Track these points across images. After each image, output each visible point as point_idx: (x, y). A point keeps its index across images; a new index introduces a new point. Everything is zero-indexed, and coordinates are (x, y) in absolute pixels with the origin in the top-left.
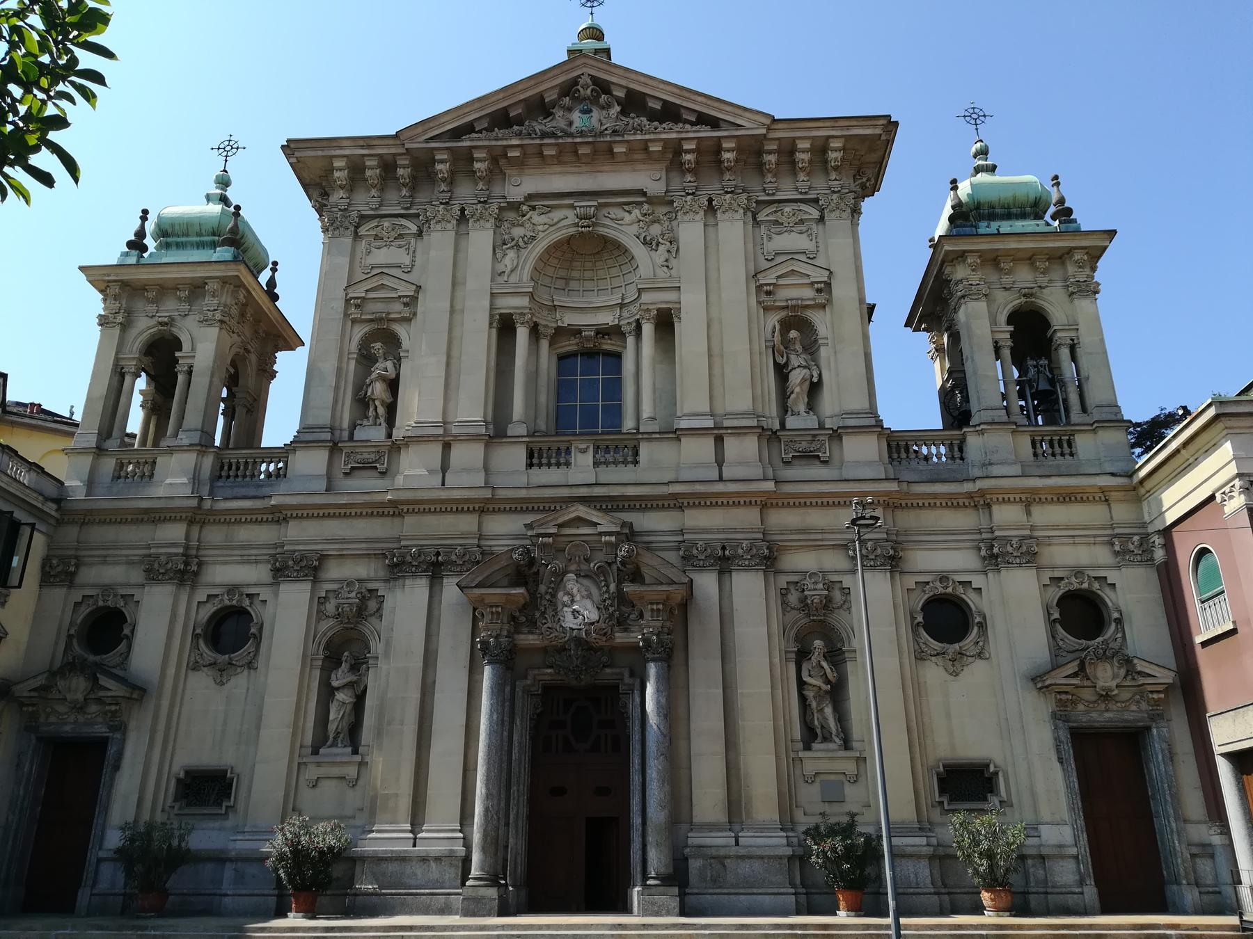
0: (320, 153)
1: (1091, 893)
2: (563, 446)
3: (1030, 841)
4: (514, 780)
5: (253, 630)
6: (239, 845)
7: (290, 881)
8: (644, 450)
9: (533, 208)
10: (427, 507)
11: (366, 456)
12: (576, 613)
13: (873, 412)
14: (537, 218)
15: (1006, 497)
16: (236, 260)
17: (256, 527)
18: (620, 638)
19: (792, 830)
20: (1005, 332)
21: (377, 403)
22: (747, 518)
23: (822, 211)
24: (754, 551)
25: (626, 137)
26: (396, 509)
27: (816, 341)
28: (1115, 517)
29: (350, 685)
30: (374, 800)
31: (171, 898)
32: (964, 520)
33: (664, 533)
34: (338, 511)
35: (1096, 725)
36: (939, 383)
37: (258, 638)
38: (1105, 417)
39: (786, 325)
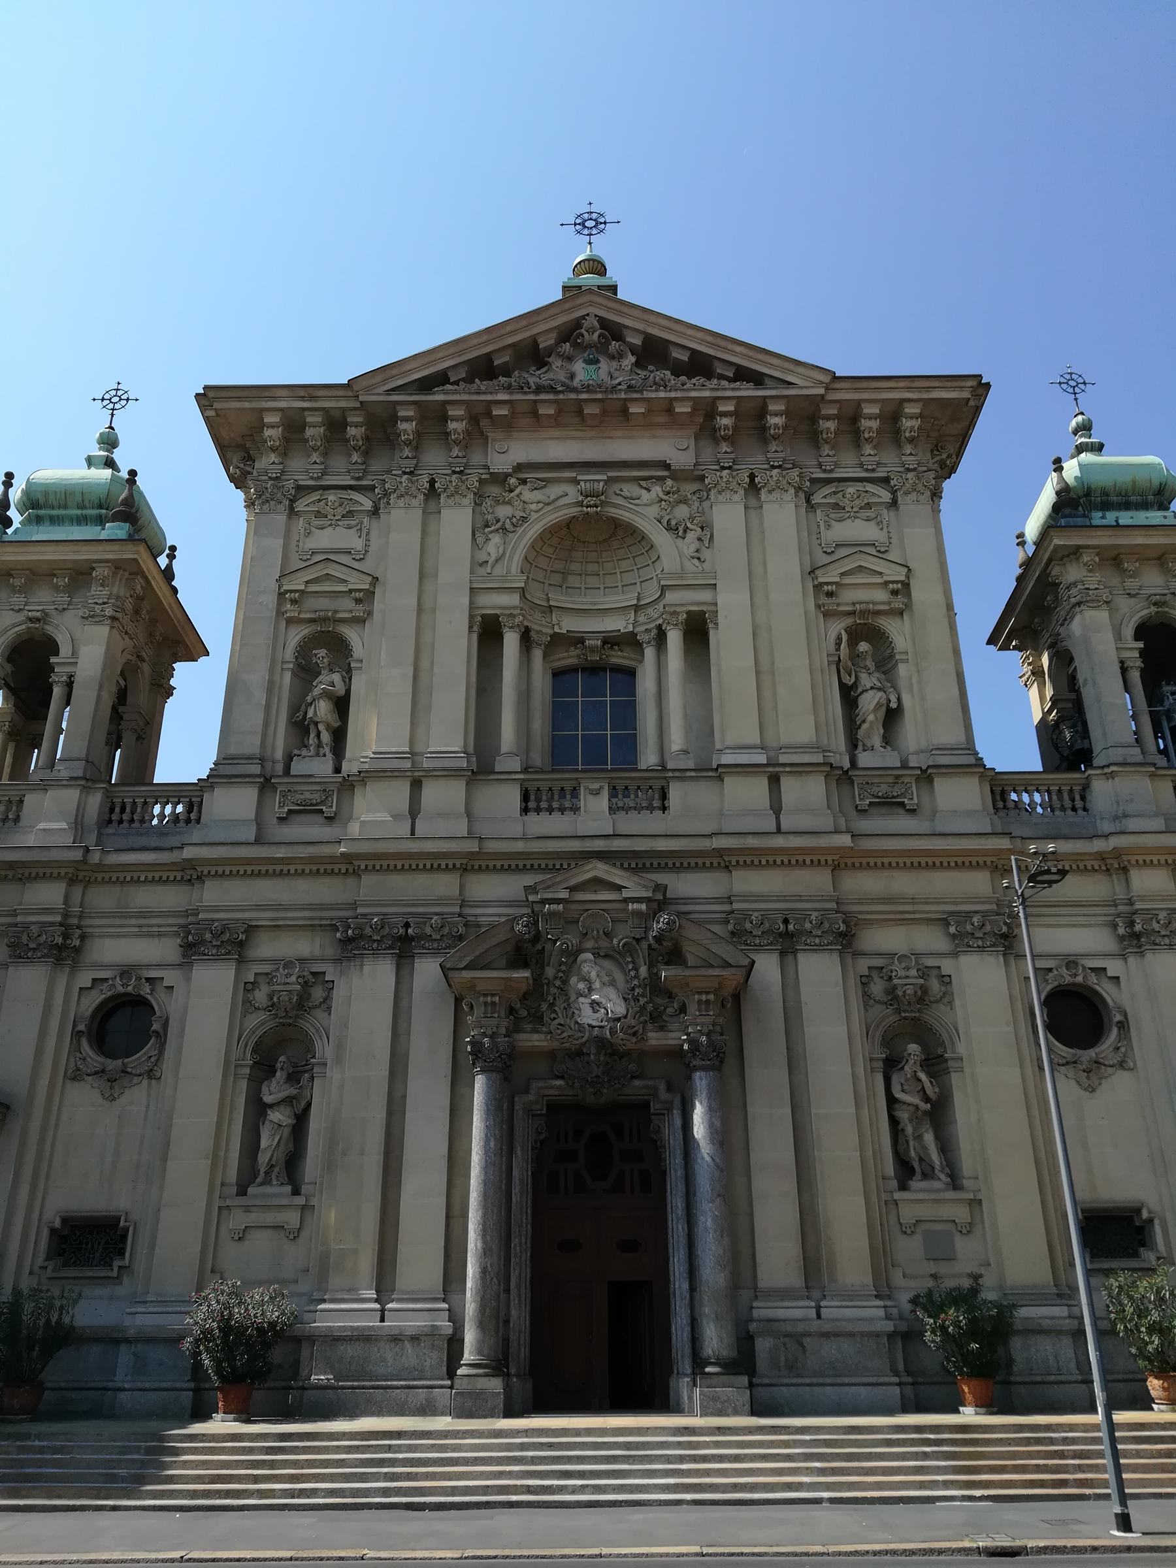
0: (246, 405)
2: (568, 786)
5: (155, 1027)
6: (140, 1320)
7: (219, 1371)
8: (675, 793)
9: (524, 482)
10: (392, 863)
11: (307, 795)
12: (595, 1005)
13: (969, 747)
14: (528, 495)
15: (1148, 859)
16: (131, 539)
17: (160, 889)
18: (655, 1039)
19: (890, 1298)
20: (1133, 649)
21: (321, 727)
22: (816, 881)
23: (894, 492)
24: (826, 925)
25: (646, 394)
26: (352, 866)
27: (892, 656)
29: (289, 1101)
34: (271, 868)
36: (1037, 716)
37: (162, 1037)
39: (855, 635)
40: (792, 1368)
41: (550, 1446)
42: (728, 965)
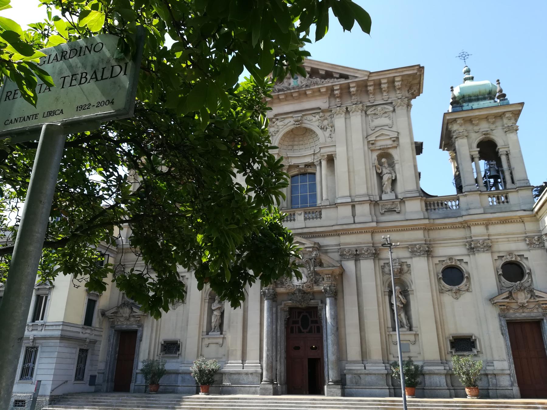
1: (516, 389)
2: (292, 213)
3: (488, 368)
4: (278, 344)
6: (183, 368)
8: (324, 212)
9: (277, 119)
18: (316, 288)
22: (366, 238)
24: (369, 251)
25: (311, 87)
27: (394, 162)
28: (527, 228)
29: (219, 308)
30: (228, 351)
31: (161, 387)
32: (459, 233)
33: (332, 246)
35: (519, 319)
36: (454, 173)
38: (524, 185)
39: (380, 157)
40: (357, 383)
41: (276, 403)
42: (334, 266)
